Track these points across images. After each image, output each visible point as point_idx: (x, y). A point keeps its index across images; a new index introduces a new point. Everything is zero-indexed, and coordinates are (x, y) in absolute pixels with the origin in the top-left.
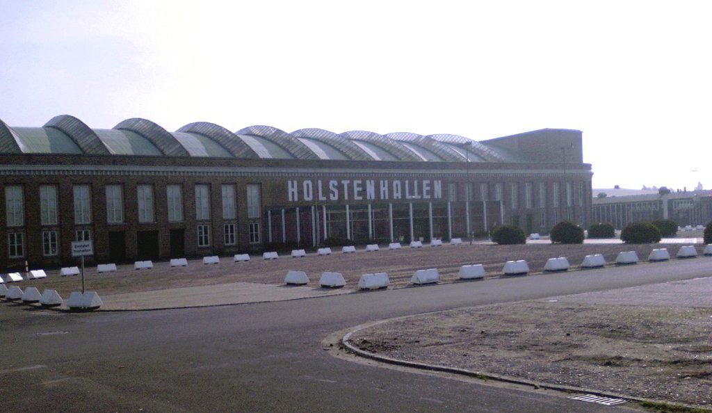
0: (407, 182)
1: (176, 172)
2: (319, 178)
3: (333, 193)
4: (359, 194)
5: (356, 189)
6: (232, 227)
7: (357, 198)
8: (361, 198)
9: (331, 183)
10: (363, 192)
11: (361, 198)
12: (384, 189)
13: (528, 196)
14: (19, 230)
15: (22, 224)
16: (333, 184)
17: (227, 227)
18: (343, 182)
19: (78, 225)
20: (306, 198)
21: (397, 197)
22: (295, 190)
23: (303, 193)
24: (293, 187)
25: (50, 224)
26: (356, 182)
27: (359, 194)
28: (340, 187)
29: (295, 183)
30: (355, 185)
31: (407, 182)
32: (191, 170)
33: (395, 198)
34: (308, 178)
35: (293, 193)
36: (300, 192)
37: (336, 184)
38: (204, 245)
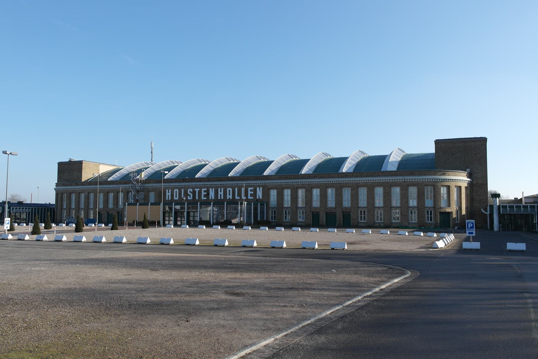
0: (236, 189)
1: (145, 186)
2: (183, 188)
3: (190, 196)
4: (205, 196)
5: (203, 193)
6: (431, 211)
7: (203, 198)
8: (206, 198)
9: (189, 190)
10: (207, 195)
11: (206, 198)
12: (221, 193)
13: (111, 201)
14: (431, 209)
15: (432, 206)
16: (190, 191)
17: (428, 212)
18: (195, 190)
19: (376, 207)
20: (175, 198)
21: (229, 198)
22: (170, 194)
23: (173, 196)
24: (169, 193)
25: (429, 206)
26: (203, 190)
27: (205, 196)
28: (194, 193)
29: (170, 190)
30: (203, 191)
31: (236, 189)
32: (272, 182)
33: (228, 198)
34: (176, 188)
35: (221, 195)
36: (172, 195)
37: (191, 190)
38: (273, 220)
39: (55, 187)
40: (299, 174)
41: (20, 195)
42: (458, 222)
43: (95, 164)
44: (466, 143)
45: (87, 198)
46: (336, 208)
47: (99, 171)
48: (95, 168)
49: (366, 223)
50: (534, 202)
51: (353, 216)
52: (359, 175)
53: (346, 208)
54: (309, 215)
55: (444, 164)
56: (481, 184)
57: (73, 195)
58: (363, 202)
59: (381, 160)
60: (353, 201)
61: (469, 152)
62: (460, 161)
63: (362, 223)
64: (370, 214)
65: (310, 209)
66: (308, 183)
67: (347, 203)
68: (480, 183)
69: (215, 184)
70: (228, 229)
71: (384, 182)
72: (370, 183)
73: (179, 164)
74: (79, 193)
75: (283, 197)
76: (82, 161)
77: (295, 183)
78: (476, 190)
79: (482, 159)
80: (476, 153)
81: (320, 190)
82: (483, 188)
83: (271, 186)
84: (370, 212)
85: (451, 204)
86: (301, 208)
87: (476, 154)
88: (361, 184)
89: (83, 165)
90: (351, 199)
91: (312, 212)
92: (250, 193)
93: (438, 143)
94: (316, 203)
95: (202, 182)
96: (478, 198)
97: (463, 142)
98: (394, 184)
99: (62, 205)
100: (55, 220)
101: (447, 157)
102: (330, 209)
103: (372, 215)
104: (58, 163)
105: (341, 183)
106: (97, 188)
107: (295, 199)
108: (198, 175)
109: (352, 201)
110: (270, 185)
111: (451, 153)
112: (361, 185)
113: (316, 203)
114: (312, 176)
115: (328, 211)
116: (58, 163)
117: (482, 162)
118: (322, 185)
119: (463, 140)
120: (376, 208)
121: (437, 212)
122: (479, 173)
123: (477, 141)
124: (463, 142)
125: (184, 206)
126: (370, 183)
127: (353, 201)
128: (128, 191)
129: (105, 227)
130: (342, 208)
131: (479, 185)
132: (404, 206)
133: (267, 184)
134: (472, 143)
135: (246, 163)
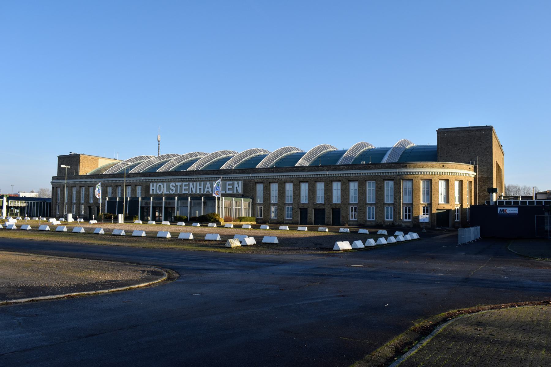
39: (52, 181)
40: (381, 162)
41: (40, 190)
42: (458, 221)
43: (94, 158)
44: (470, 132)
45: (79, 193)
46: (325, 204)
47: (98, 165)
48: (94, 162)
49: (357, 221)
50: (547, 198)
51: (343, 213)
52: (350, 167)
53: (335, 204)
54: (296, 211)
55: (447, 156)
56: (486, 178)
57: (91, 188)
58: (336, 198)
59: (340, 154)
60: (343, 197)
61: (474, 142)
62: (464, 153)
63: (353, 221)
64: (361, 212)
65: (298, 206)
66: (296, 176)
67: (336, 198)
68: (486, 177)
69: (200, 178)
70: (193, 227)
71: (377, 176)
72: (361, 177)
73: (235, 155)
74: (72, 187)
75: (269, 192)
76: (80, 154)
77: (283, 177)
78: (481, 185)
79: (487, 150)
80: (481, 143)
81: (309, 184)
82: (489, 183)
83: (257, 180)
84: (361, 209)
85: (450, 200)
86: (260, 204)
87: (481, 144)
88: (352, 177)
89: (81, 158)
90: (341, 195)
91: (300, 209)
92: (228, 187)
93: (440, 132)
94: (304, 199)
95: (188, 175)
96: (483, 194)
97: (467, 132)
98: (387, 177)
99: (56, 200)
100: (51, 215)
101: (450, 148)
102: (318, 206)
103: (363, 212)
104: (58, 157)
105: (331, 177)
106: (124, 180)
107: (282, 194)
108: (223, 167)
109: (342, 197)
110: (256, 179)
111: (454, 143)
112: (352, 179)
113: (304, 199)
114: (300, 169)
115: (317, 207)
116: (58, 157)
117: (488, 153)
118: (310, 178)
119: (478, 128)
120: (368, 205)
121: (108, 226)
122: (484, 166)
123: (482, 130)
124: (467, 132)
125: (161, 201)
126: (361, 177)
127: (343, 197)
128: (116, 185)
129: (75, 222)
130: (331, 205)
131: (484, 179)
132: (362, 204)
133: (254, 178)
134: (477, 132)
135: (278, 154)
